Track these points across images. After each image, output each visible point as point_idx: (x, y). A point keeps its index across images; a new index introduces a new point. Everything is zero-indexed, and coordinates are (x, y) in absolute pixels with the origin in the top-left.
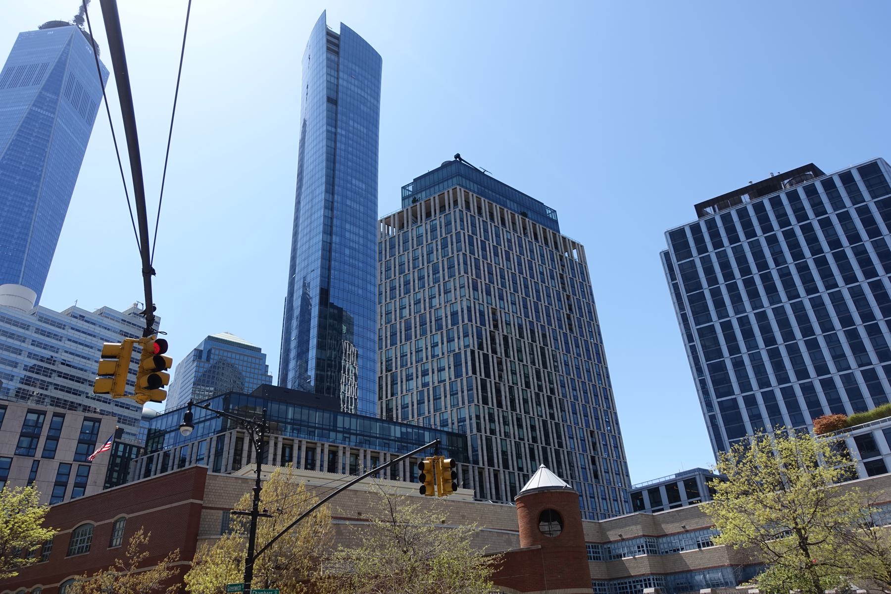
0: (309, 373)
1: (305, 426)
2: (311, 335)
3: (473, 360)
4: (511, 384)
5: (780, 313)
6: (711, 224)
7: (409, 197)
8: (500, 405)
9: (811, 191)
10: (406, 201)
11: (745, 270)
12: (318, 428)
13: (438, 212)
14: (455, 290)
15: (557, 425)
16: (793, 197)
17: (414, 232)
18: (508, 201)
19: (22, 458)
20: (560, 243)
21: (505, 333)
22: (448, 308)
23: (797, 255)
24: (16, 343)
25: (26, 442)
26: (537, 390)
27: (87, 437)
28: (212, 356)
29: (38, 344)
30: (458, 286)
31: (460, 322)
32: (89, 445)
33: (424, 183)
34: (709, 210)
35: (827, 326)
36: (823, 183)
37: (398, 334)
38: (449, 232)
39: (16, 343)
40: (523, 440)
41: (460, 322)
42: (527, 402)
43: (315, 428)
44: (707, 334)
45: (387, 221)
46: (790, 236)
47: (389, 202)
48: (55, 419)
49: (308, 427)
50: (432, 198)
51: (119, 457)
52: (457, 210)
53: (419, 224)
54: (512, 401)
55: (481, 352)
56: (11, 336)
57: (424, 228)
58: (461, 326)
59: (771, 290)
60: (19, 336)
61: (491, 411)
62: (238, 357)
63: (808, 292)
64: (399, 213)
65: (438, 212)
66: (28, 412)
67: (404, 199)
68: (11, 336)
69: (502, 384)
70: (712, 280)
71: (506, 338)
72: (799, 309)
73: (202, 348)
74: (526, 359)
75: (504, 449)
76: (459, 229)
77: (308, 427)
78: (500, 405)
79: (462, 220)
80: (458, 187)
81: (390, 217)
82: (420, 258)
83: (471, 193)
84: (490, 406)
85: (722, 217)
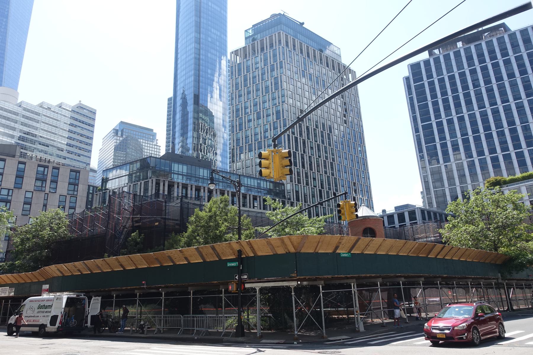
0: (188, 146)
1: (193, 177)
2: (189, 123)
3: (289, 140)
4: (310, 155)
5: (472, 117)
6: (437, 61)
7: (249, 37)
8: (303, 166)
9: (501, 41)
10: (248, 39)
11: (455, 90)
12: (201, 178)
13: (268, 47)
14: (279, 98)
15: (335, 179)
16: (489, 44)
17: (253, 60)
18: (298, 34)
19: (38, 193)
20: (342, 70)
21: (308, 125)
22: (274, 109)
23: (487, 81)
24: (12, 124)
25: (39, 183)
26: (325, 159)
27: (40, 176)
28: (124, 134)
29: (25, 125)
30: (280, 96)
31: (282, 117)
32: (75, 185)
33: (259, 29)
34: (436, 51)
35: (499, 125)
36: (509, 35)
37: (244, 124)
38: (275, 61)
39: (12, 124)
40: (316, 187)
41: (282, 117)
42: (319, 166)
43: (200, 178)
44: (428, 128)
45: (236, 53)
46: (484, 69)
47: (236, 40)
48: (54, 170)
49: (195, 177)
50: (265, 38)
51: (91, 193)
52: (281, 47)
53: (256, 55)
54: (311, 165)
55: (293, 136)
56: (8, 119)
57: (260, 57)
58: (282, 120)
59: (469, 102)
60: (12, 119)
61: (299, 171)
62: (140, 134)
63: (491, 105)
64: (243, 48)
65: (268, 47)
66: (19, 163)
67: (246, 38)
68: (8, 119)
69: (305, 155)
70: (434, 96)
71: (308, 128)
72: (484, 115)
73: (118, 128)
74: (319, 139)
75: (297, 190)
76: (281, 60)
77: (195, 177)
78: (303, 166)
79: (283, 54)
80: (282, 32)
81: (238, 50)
82: (257, 77)
83: (289, 36)
84: (298, 167)
85: (444, 56)
